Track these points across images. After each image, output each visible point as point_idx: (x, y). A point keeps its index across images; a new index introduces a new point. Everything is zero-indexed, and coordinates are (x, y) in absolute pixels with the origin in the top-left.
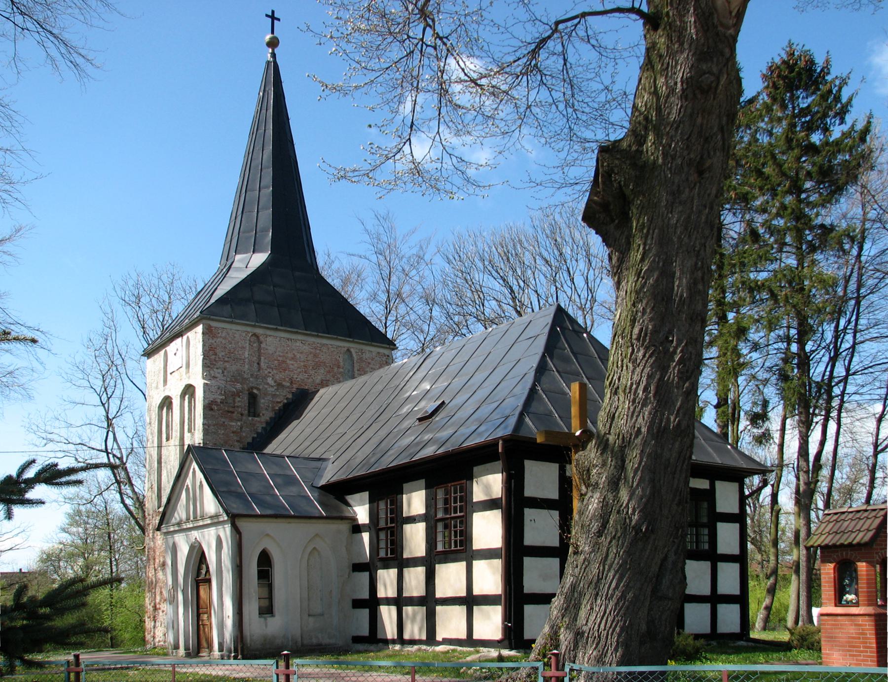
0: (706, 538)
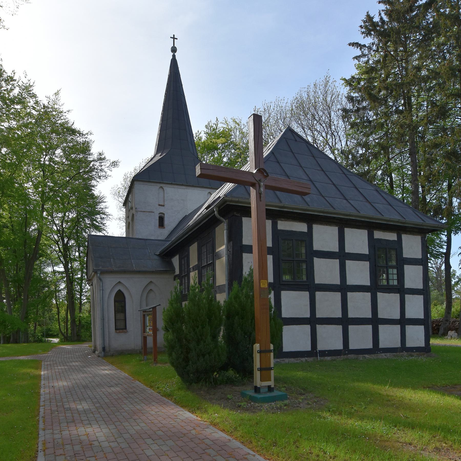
0: (395, 277)
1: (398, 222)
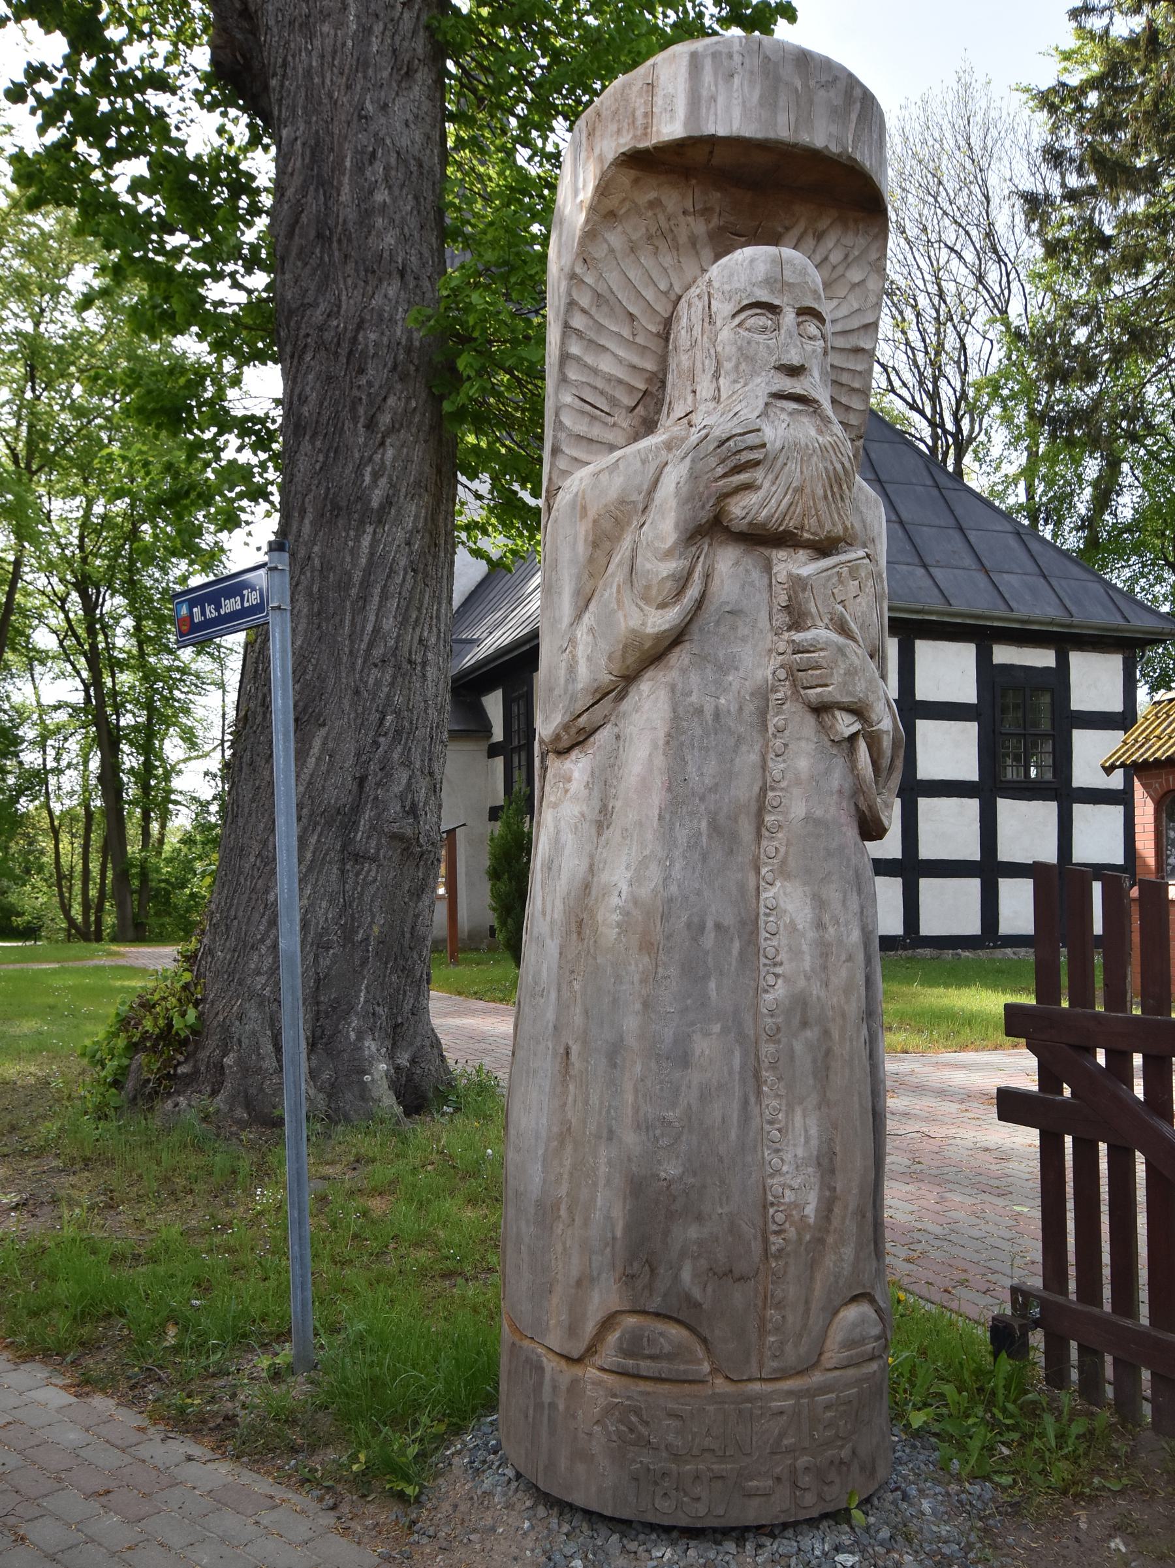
1: (1051, 623)
